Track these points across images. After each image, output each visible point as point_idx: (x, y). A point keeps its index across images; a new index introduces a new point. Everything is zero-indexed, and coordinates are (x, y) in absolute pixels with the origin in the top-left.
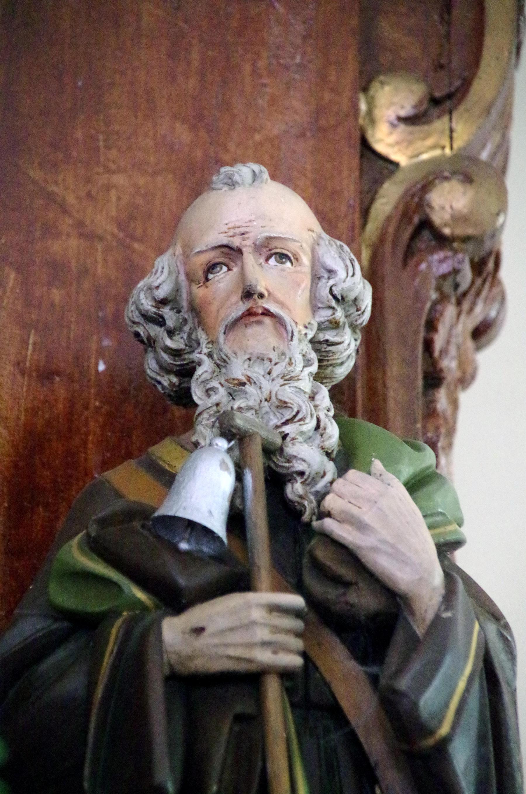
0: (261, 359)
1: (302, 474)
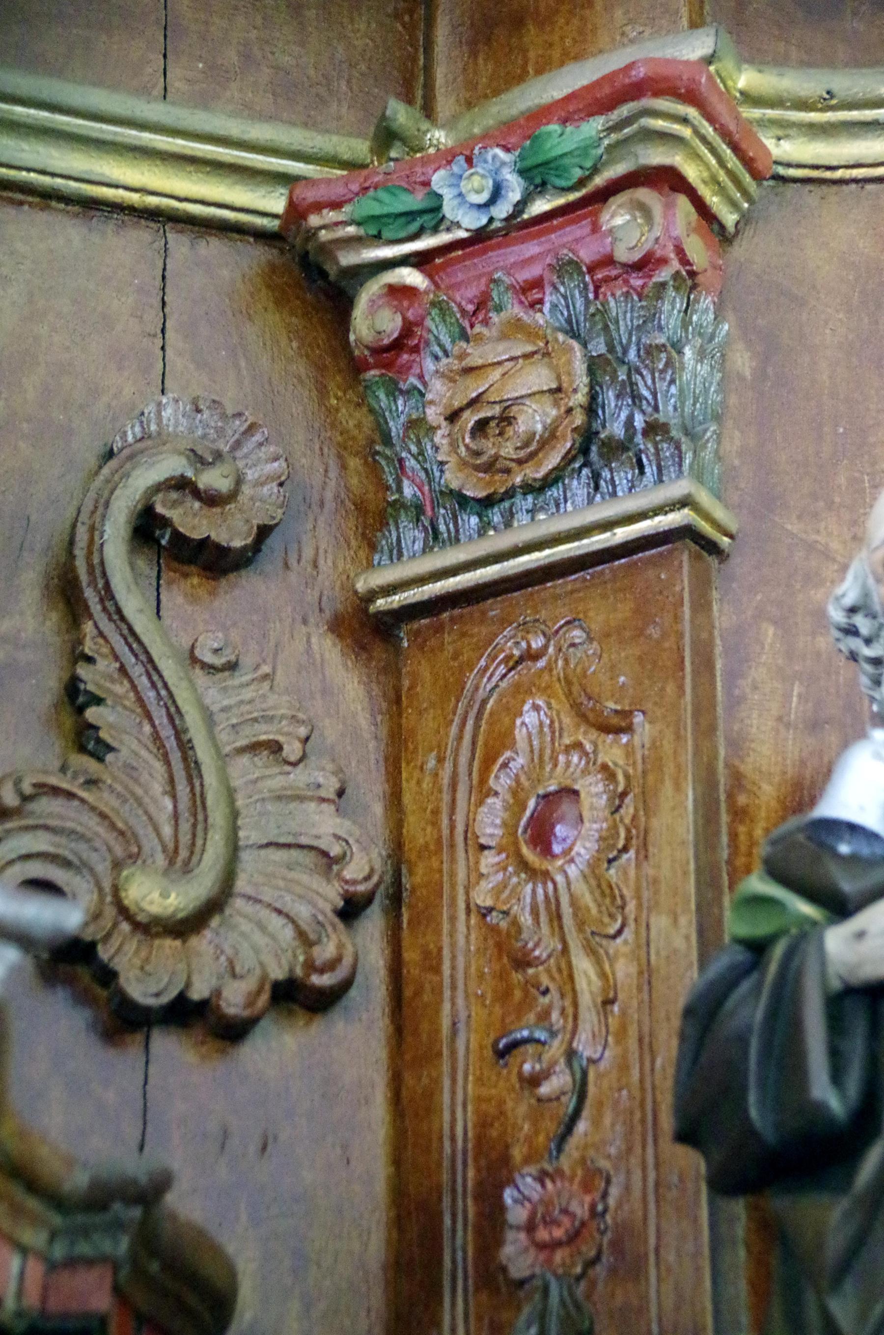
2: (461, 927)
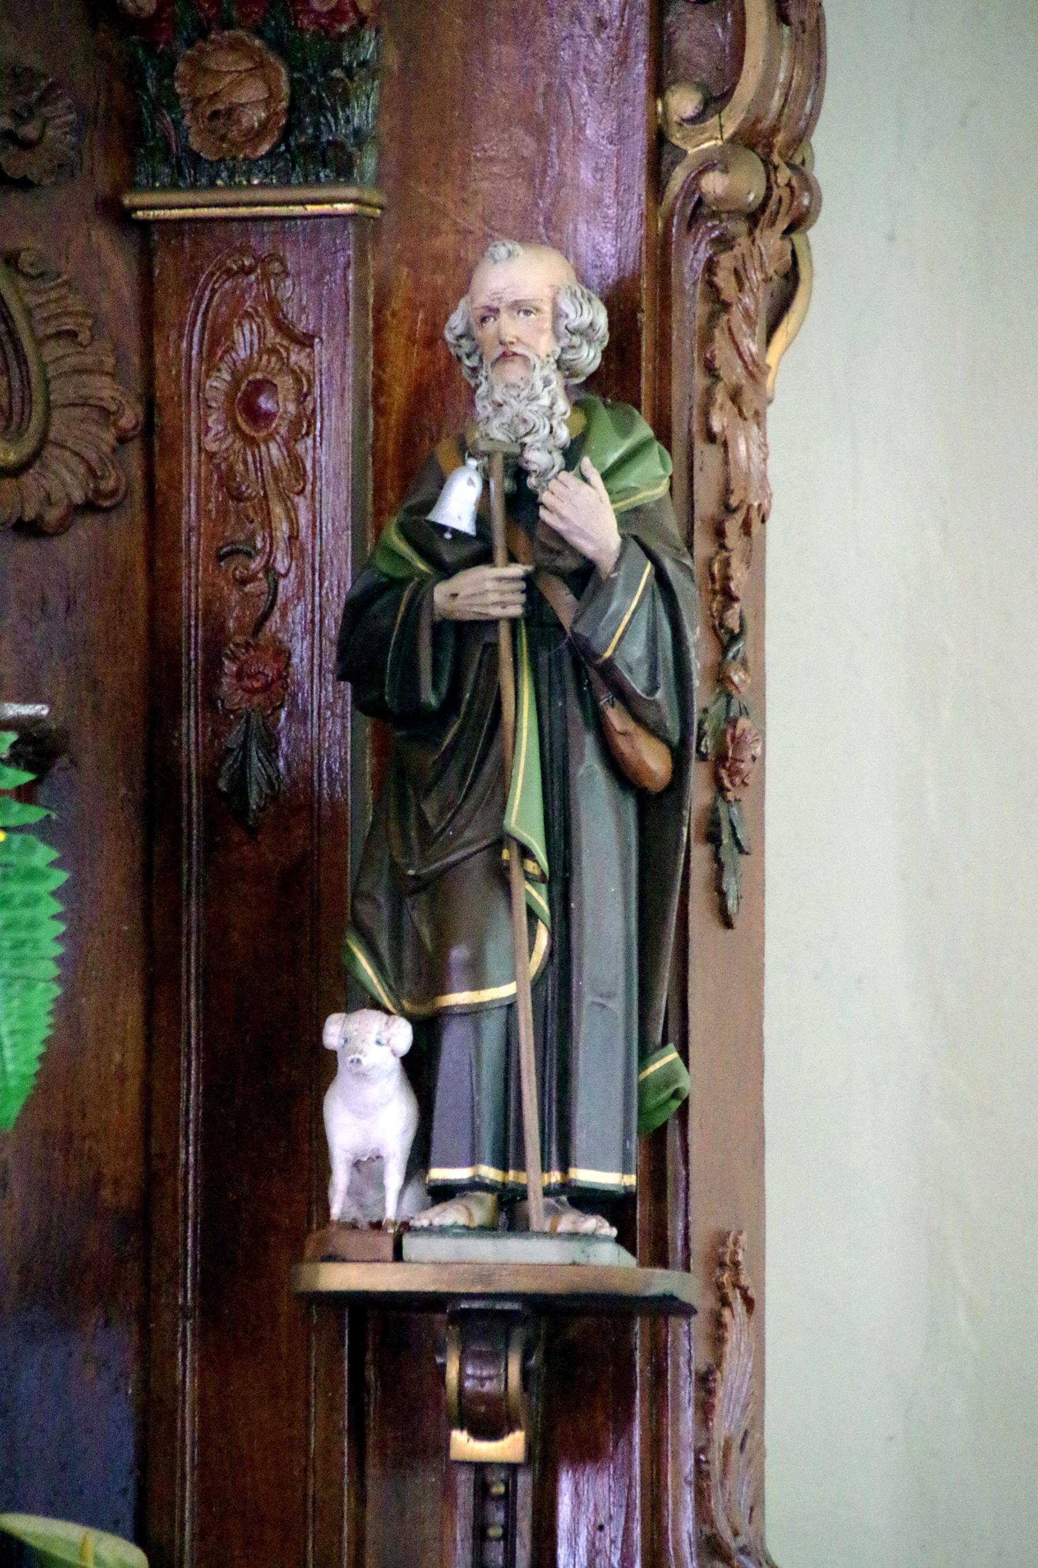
0: (514, 386)
1: (535, 471)
2: (194, 459)
